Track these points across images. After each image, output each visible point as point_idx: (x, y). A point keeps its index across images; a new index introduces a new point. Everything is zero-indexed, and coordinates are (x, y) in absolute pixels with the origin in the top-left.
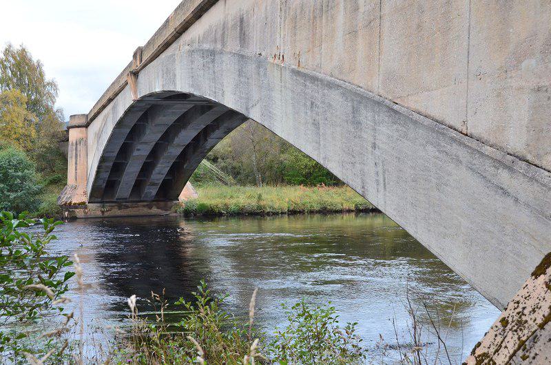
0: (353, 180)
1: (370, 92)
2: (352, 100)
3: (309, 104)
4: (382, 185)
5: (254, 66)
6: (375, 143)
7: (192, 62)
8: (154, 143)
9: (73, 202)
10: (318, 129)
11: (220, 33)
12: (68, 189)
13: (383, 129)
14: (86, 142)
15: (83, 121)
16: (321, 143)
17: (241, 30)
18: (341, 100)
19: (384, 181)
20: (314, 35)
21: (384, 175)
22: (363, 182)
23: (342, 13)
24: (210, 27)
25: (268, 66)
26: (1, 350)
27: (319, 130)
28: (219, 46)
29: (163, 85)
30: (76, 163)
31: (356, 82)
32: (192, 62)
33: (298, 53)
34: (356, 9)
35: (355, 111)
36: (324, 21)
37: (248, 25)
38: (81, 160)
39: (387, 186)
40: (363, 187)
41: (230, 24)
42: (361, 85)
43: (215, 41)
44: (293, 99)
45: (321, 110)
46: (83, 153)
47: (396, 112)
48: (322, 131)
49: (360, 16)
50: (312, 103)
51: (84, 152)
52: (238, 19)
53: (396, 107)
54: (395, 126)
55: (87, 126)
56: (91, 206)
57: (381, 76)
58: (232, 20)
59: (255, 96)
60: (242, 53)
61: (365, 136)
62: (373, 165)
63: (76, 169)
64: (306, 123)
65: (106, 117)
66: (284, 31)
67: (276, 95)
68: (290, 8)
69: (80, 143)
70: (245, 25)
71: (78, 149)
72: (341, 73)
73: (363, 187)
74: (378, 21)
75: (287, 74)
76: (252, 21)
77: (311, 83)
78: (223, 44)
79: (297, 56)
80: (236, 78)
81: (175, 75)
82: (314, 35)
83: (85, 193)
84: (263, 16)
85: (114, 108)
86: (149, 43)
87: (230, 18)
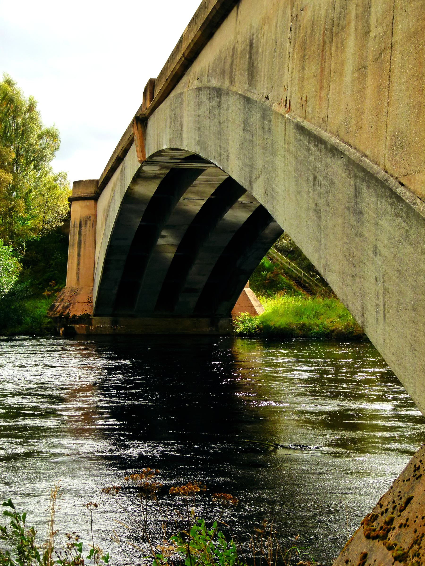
0: (353, 303)
1: (376, 164)
2: (355, 177)
3: (311, 178)
4: (382, 312)
5: (259, 116)
6: (376, 247)
7: (199, 105)
8: (186, 227)
9: (72, 315)
10: (320, 218)
11: (229, 60)
12: (66, 293)
13: (384, 223)
14: (95, 222)
15: (91, 191)
16: (323, 241)
17: (250, 57)
18: (344, 175)
19: (384, 305)
20: (322, 70)
21: (384, 298)
22: (363, 304)
23: (352, 37)
24: (220, 51)
25: (273, 117)
26: (294, 563)
27: (320, 220)
28: (227, 84)
29: (171, 140)
30: (79, 255)
31: (362, 148)
32: (199, 105)
33: (305, 98)
34: (367, 32)
35: (357, 193)
36: (334, 48)
37: (257, 52)
38: (86, 250)
39: (388, 315)
40: (363, 315)
41: (240, 47)
42: (367, 152)
43: (223, 74)
44: (296, 170)
45: (323, 190)
46: (90, 239)
47: (399, 198)
48: (323, 223)
49: (371, 43)
50: (315, 178)
51: (91, 238)
52: (248, 42)
53: (400, 190)
54: (398, 220)
55: (95, 198)
56: (96, 320)
57: (388, 139)
58: (242, 42)
59: (259, 164)
60: (249, 95)
61: (366, 234)
62: (373, 281)
63: (78, 264)
64: (309, 209)
65: (115, 185)
66: (293, 63)
67: (279, 162)
68: (300, 26)
69: (86, 223)
70: (254, 51)
71: (83, 233)
72: (347, 132)
73: (363, 315)
74: (389, 51)
75: (291, 129)
76: (261, 45)
77: (315, 146)
78: (232, 82)
79: (304, 103)
80: (241, 133)
81: (182, 125)
82: (322, 70)
83: (90, 300)
84: (273, 38)
85: (122, 172)
86: (162, 74)
87: (240, 39)
